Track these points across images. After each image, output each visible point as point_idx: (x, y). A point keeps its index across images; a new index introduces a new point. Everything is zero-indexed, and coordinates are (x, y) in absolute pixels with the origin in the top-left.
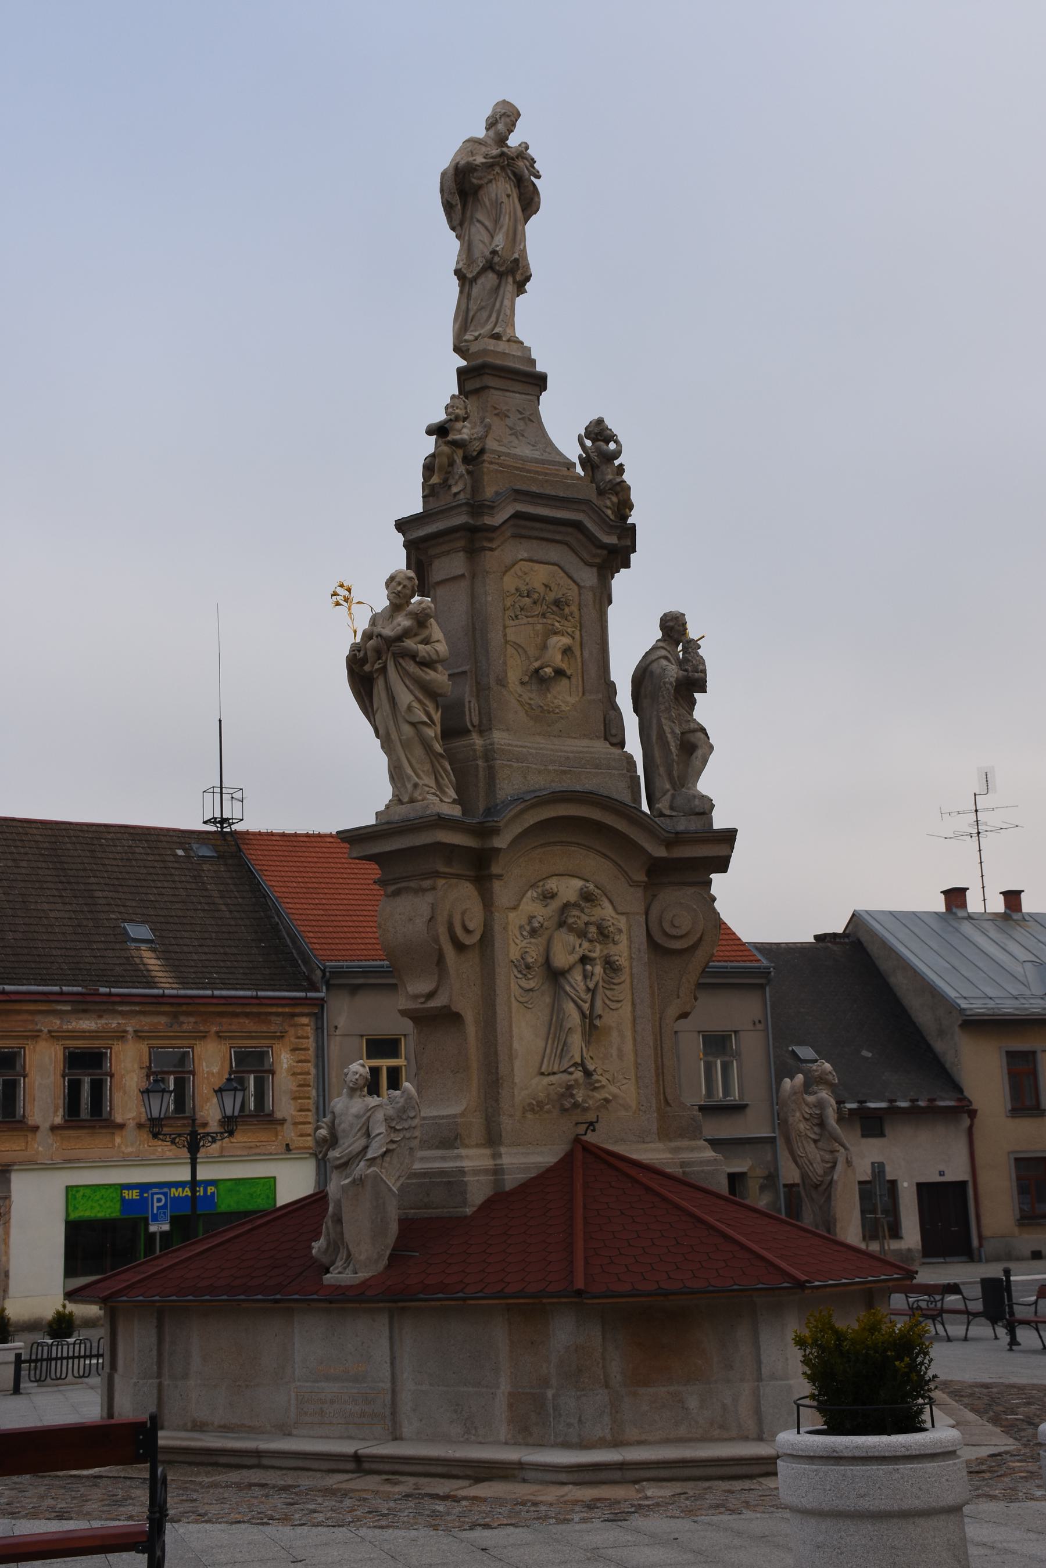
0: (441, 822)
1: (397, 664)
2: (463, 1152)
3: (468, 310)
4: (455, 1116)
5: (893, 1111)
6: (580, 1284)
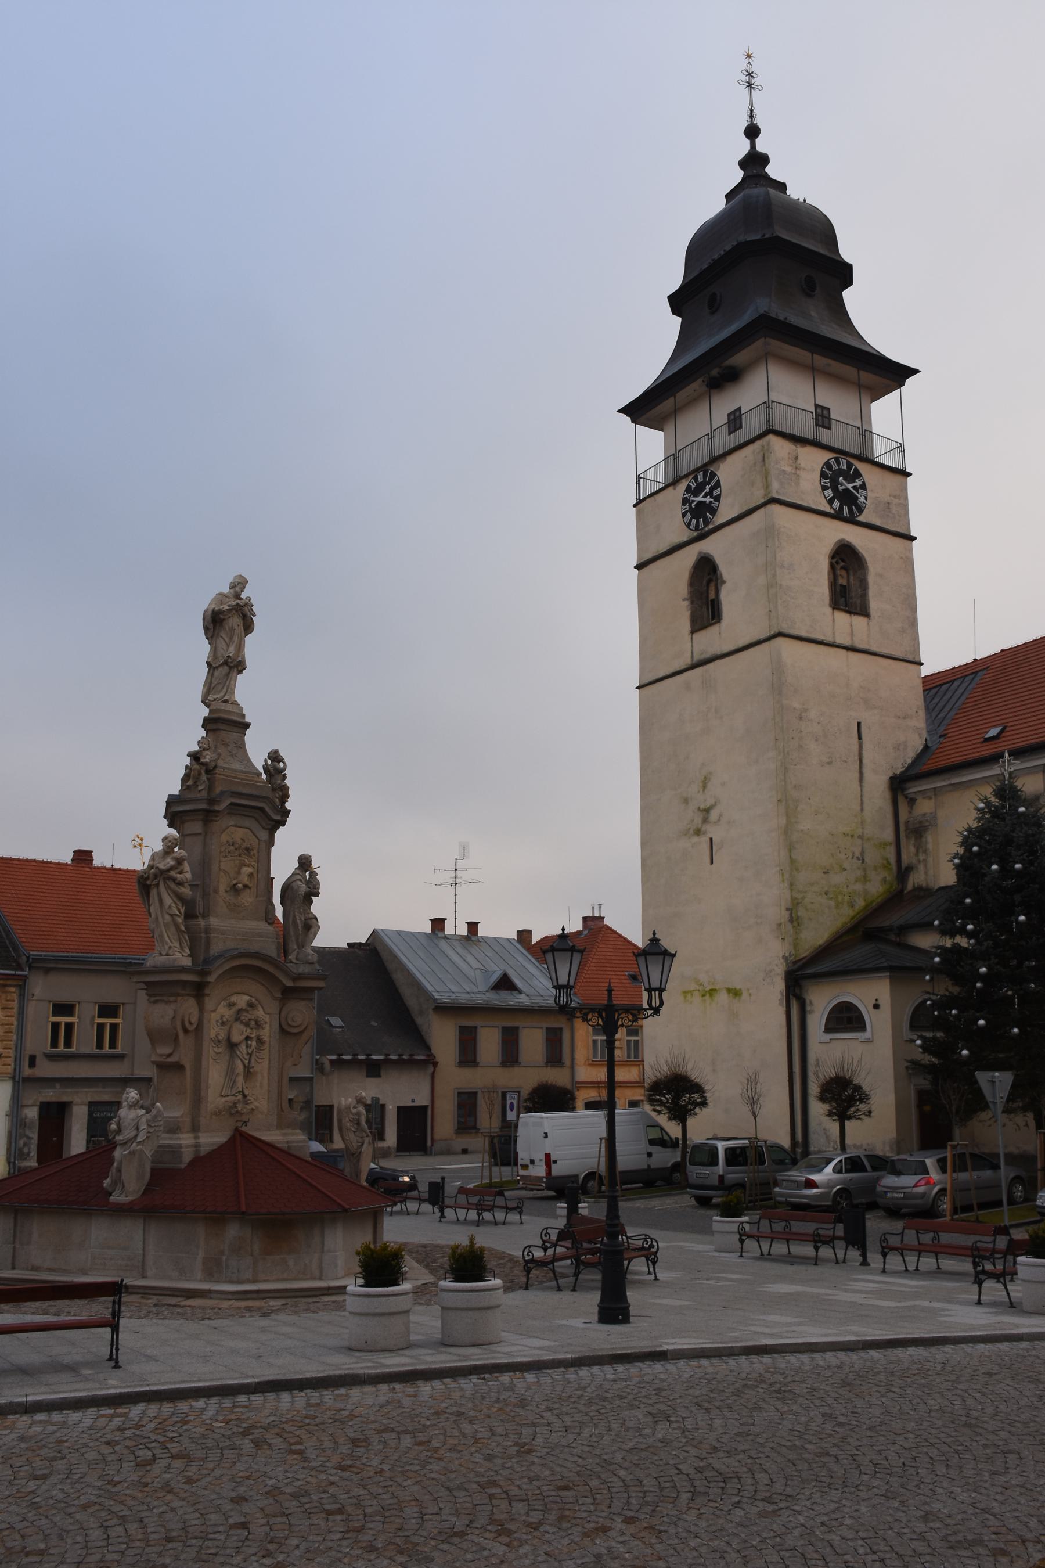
0: (183, 970)
1: (165, 883)
2: (181, 1136)
3: (211, 683)
4: (177, 1117)
5: (387, 1061)
6: (244, 1209)
